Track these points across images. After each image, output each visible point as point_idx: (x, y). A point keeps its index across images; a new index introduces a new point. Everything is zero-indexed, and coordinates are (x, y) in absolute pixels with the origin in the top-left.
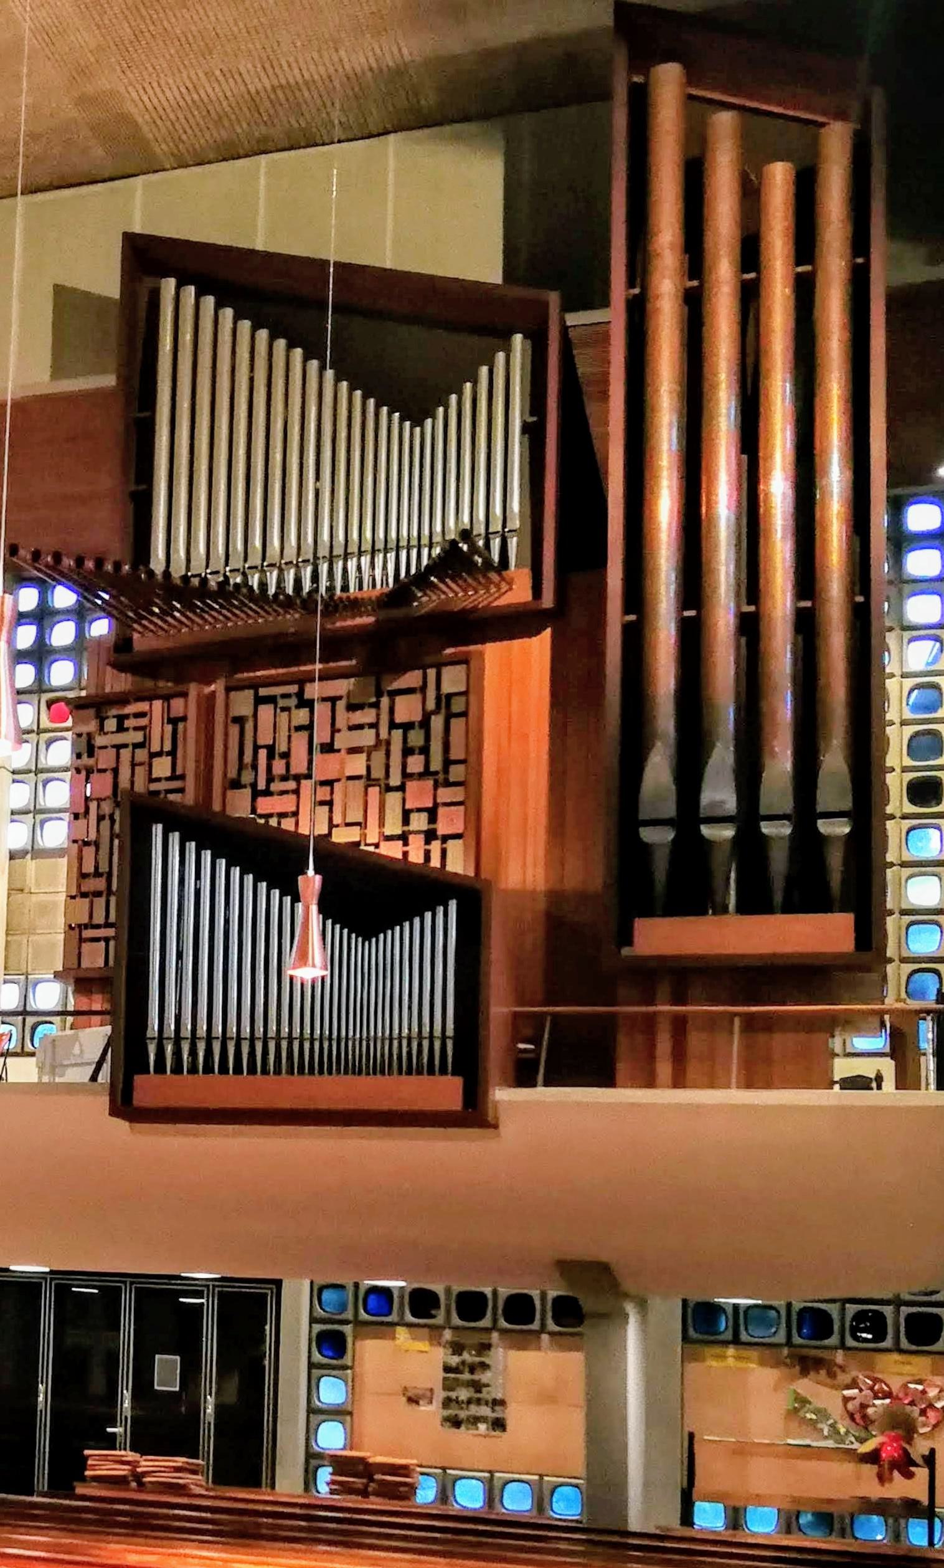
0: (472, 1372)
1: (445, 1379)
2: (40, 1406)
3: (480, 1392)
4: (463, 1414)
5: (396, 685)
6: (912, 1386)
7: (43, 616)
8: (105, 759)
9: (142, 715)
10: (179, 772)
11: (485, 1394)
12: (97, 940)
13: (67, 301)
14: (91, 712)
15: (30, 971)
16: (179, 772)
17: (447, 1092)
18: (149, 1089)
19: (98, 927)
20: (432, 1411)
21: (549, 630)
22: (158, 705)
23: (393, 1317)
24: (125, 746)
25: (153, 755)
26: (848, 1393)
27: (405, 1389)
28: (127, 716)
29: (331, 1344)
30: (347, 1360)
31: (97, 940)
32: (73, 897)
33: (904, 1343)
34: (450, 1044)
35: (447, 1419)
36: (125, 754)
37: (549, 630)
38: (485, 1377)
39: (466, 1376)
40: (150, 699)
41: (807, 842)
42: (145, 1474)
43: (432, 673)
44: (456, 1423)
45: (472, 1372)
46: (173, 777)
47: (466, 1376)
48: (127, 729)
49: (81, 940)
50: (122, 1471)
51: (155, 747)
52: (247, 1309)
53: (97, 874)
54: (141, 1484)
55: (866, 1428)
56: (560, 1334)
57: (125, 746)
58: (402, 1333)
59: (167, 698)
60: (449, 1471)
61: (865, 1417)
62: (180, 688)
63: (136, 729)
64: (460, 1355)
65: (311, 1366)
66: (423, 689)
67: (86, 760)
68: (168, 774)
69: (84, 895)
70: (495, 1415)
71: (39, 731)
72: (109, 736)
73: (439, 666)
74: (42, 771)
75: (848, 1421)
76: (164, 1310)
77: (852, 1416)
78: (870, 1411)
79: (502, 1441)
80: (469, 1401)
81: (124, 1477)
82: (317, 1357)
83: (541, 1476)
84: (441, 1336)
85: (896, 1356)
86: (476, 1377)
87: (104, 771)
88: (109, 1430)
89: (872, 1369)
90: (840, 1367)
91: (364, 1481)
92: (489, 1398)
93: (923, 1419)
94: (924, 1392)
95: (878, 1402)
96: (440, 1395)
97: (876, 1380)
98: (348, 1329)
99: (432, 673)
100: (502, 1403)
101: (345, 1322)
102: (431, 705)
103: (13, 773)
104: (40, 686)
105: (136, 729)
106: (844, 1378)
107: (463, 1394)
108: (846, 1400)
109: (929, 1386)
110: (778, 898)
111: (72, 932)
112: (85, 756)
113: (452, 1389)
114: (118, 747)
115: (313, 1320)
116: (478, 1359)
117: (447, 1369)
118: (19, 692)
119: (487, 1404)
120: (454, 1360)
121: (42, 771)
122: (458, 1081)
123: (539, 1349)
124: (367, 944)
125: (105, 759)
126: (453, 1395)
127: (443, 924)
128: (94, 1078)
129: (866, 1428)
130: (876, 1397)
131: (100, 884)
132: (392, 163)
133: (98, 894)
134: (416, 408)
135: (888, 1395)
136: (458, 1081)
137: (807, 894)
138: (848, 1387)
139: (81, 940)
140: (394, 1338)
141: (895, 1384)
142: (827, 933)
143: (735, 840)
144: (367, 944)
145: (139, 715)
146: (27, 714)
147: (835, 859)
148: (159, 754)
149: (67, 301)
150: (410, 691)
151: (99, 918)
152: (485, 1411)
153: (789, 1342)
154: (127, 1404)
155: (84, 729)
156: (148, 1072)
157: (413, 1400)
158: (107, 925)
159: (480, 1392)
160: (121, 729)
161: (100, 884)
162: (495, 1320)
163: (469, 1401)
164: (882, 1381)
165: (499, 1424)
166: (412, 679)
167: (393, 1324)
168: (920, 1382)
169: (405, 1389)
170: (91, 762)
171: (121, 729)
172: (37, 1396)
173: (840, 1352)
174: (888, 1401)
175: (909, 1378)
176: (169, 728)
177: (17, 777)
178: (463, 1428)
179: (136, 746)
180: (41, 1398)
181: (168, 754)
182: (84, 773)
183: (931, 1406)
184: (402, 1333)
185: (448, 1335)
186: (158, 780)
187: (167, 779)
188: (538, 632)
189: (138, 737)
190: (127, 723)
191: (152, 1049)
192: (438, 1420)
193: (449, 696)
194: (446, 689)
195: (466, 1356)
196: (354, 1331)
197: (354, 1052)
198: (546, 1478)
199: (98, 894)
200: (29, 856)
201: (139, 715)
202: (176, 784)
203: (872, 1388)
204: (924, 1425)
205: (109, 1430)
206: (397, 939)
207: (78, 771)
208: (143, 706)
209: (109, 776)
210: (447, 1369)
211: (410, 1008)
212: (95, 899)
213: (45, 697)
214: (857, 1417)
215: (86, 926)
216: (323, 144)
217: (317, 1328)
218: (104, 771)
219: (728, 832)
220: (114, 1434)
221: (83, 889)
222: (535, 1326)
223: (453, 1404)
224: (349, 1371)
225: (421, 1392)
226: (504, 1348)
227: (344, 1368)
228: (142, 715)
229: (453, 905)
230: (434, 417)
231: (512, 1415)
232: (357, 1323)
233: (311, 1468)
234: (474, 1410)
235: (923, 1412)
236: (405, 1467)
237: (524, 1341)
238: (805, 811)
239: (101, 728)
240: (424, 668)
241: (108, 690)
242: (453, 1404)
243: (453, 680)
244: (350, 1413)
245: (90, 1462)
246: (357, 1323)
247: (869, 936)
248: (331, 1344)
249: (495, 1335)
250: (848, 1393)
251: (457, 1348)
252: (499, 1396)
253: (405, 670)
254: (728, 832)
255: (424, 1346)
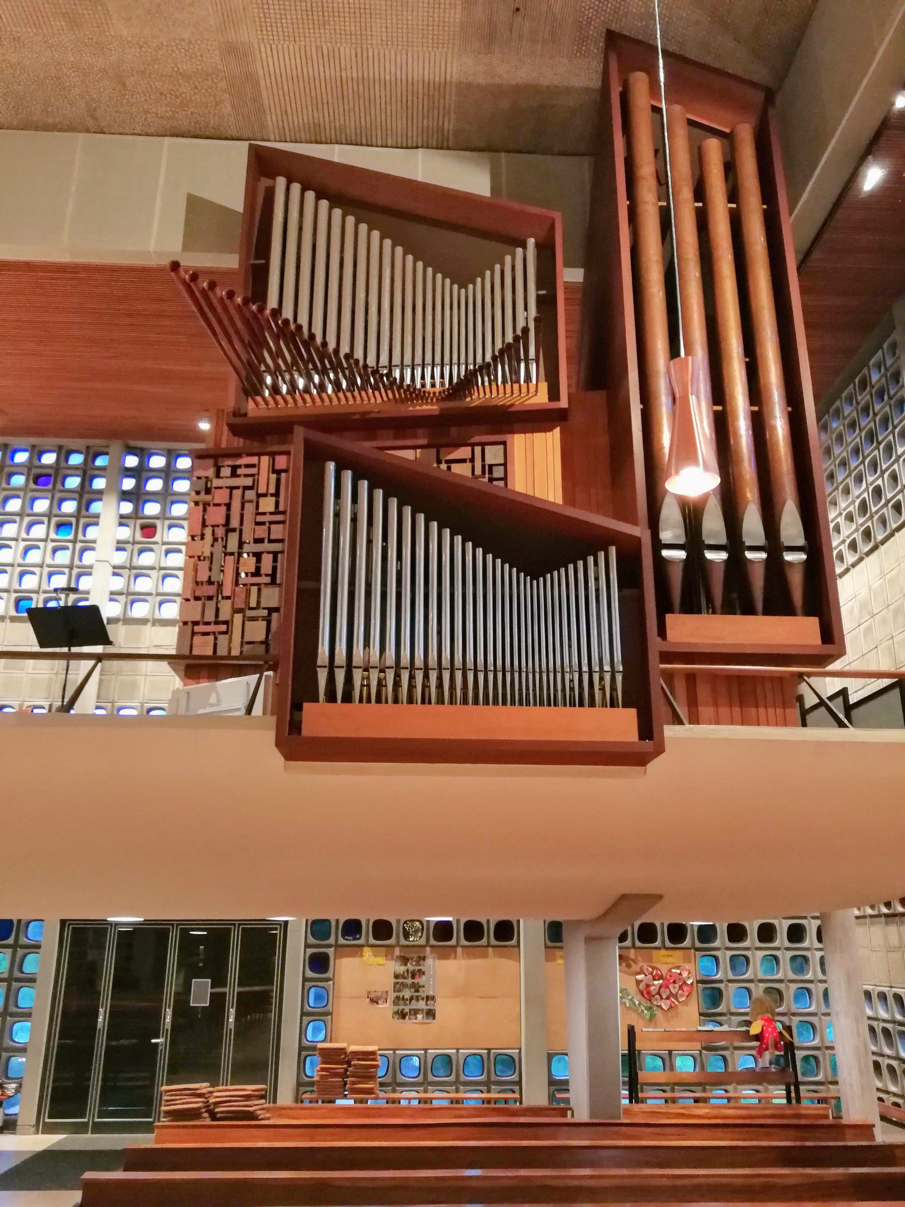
0: (413, 977)
1: (396, 984)
2: (100, 1025)
3: (417, 991)
4: (407, 1009)
5: (451, 457)
6: (674, 971)
7: (141, 473)
8: (221, 496)
9: (253, 466)
10: (281, 508)
11: (423, 993)
12: (207, 634)
13: (196, 206)
14: (211, 462)
15: (116, 699)
16: (281, 508)
17: (622, 725)
18: (319, 719)
19: (208, 623)
20: (387, 1008)
21: (558, 428)
22: (265, 460)
23: (362, 941)
24: (238, 488)
25: (259, 496)
26: (639, 977)
27: (369, 992)
28: (240, 466)
29: (319, 963)
30: (330, 974)
31: (207, 634)
32: (187, 600)
33: (668, 944)
34: (619, 678)
35: (397, 1013)
36: (237, 493)
37: (558, 428)
38: (421, 980)
39: (409, 981)
40: (259, 455)
41: (775, 566)
42: (216, 1104)
43: (478, 449)
44: (403, 1015)
45: (413, 977)
46: (277, 512)
47: (409, 981)
48: (239, 476)
49: (193, 634)
50: (195, 1103)
51: (262, 490)
52: (263, 942)
53: (210, 582)
54: (213, 1116)
55: (650, 1001)
56: (499, 946)
57: (238, 488)
58: (367, 951)
59: (272, 455)
60: (397, 1052)
61: (649, 993)
62: (283, 448)
63: (246, 476)
64: (406, 965)
65: (305, 980)
66: (472, 460)
67: (203, 497)
68: (272, 510)
69: (197, 598)
70: (428, 1007)
71: (134, 543)
72: (225, 480)
73: (483, 445)
74: (135, 568)
75: (639, 996)
76: (207, 947)
77: (642, 993)
78: (652, 988)
79: (435, 1024)
80: (411, 998)
81: (199, 1109)
82: (310, 974)
83: (458, 1050)
84: (393, 952)
85: (663, 952)
86: (416, 981)
87: (219, 505)
88: (153, 1041)
89: (651, 961)
90: (632, 960)
91: (345, 1066)
92: (424, 995)
93: (681, 992)
94: (680, 974)
95: (656, 982)
96: (392, 996)
97: (653, 968)
98: (331, 951)
99: (478, 449)
100: (433, 998)
101: (329, 946)
102: (478, 471)
103: (114, 567)
104: (137, 514)
105: (246, 476)
106: (635, 968)
107: (407, 993)
108: (638, 982)
109: (683, 970)
110: (759, 605)
111: (185, 627)
112: (203, 493)
113: (399, 991)
114: (232, 488)
115: (307, 946)
116: (417, 968)
117: (397, 976)
118: (122, 517)
119: (423, 999)
120: (401, 969)
121: (135, 568)
122: (632, 713)
123: (455, 958)
124: (535, 582)
125: (221, 496)
126: (401, 994)
127: (603, 570)
128: (249, 710)
129: (650, 1001)
130: (654, 979)
131: (211, 590)
132: (420, 164)
133: (210, 598)
134: (463, 278)
135: (661, 977)
136: (632, 713)
137: (778, 603)
138: (638, 973)
139: (193, 634)
140: (361, 956)
141: (664, 970)
142: (801, 631)
143: (727, 562)
144: (535, 582)
145: (248, 466)
146: (125, 533)
147: (796, 580)
148: (265, 495)
149: (196, 206)
150: (463, 461)
151: (210, 616)
152: (421, 1005)
153: (634, 946)
154: (168, 1019)
155: (202, 473)
156: (317, 701)
157: (374, 1001)
158: (217, 623)
159: (417, 991)
160: (234, 474)
161: (211, 590)
162: (428, 940)
163: (411, 998)
164: (657, 969)
165: (431, 1014)
166: (463, 452)
167: (362, 946)
168: (678, 967)
169: (369, 992)
170: (208, 498)
171: (234, 474)
172: (97, 1017)
173: (632, 951)
174: (661, 981)
175: (671, 966)
176: (273, 477)
177: (116, 570)
178: (407, 1017)
179: (246, 488)
180: (100, 1019)
181: (272, 495)
182: (201, 507)
183: (685, 983)
184: (367, 951)
185: (397, 952)
186: (264, 514)
187: (271, 513)
188: (551, 429)
189: (248, 482)
190: (239, 471)
191: (322, 677)
192: (390, 1014)
193: (491, 466)
194: (489, 460)
195: (410, 967)
196: (335, 950)
197: (520, 689)
198: (461, 1051)
199: (210, 598)
200: (121, 623)
201: (248, 466)
202: (279, 518)
203: (651, 973)
204: (682, 996)
205: (153, 1041)
206: (561, 581)
207: (197, 503)
208: (254, 460)
209: (223, 509)
210: (397, 976)
211: (570, 646)
212: (208, 602)
213: (139, 522)
214: (645, 994)
215: (196, 623)
216: (377, 146)
217: (310, 951)
218: (219, 505)
219: (723, 556)
220: (157, 1044)
221: (198, 594)
222: (453, 942)
223: (401, 1002)
224: (331, 982)
225: (379, 994)
226: (434, 959)
227: (328, 980)
228: (253, 466)
229: (613, 550)
230: (474, 284)
231: (439, 1007)
232: (337, 946)
233: (302, 1058)
234: (415, 1005)
235: (681, 988)
236: (373, 1053)
237: (446, 954)
238: (773, 544)
239: (218, 476)
240: (473, 445)
241: (224, 445)
242: (401, 1002)
243: (494, 455)
244: (330, 1014)
245: (165, 1098)
246: (337, 946)
247: (830, 633)
248: (319, 963)
249: (428, 949)
250: (639, 977)
251: (405, 960)
252: (431, 993)
253: (458, 445)
254: (723, 556)
255: (381, 960)
